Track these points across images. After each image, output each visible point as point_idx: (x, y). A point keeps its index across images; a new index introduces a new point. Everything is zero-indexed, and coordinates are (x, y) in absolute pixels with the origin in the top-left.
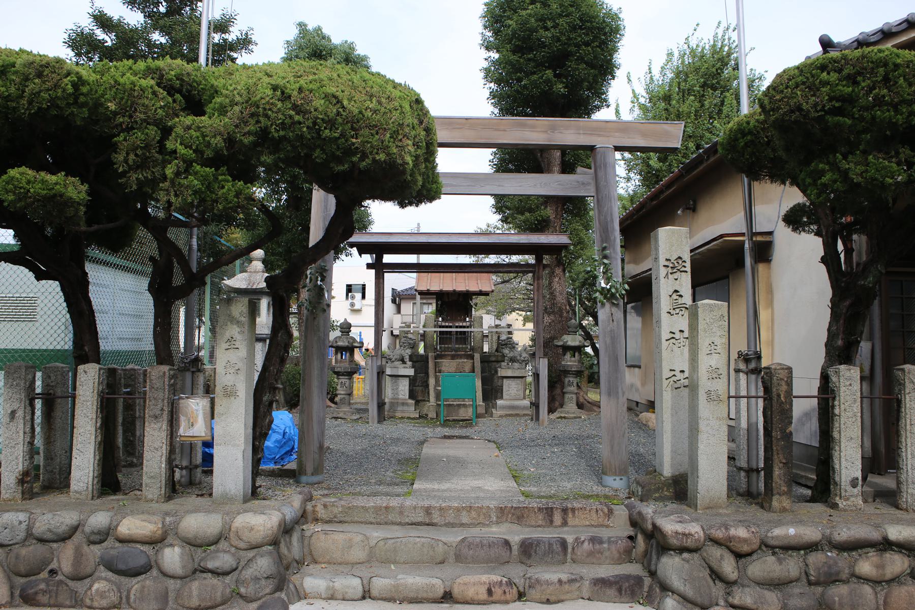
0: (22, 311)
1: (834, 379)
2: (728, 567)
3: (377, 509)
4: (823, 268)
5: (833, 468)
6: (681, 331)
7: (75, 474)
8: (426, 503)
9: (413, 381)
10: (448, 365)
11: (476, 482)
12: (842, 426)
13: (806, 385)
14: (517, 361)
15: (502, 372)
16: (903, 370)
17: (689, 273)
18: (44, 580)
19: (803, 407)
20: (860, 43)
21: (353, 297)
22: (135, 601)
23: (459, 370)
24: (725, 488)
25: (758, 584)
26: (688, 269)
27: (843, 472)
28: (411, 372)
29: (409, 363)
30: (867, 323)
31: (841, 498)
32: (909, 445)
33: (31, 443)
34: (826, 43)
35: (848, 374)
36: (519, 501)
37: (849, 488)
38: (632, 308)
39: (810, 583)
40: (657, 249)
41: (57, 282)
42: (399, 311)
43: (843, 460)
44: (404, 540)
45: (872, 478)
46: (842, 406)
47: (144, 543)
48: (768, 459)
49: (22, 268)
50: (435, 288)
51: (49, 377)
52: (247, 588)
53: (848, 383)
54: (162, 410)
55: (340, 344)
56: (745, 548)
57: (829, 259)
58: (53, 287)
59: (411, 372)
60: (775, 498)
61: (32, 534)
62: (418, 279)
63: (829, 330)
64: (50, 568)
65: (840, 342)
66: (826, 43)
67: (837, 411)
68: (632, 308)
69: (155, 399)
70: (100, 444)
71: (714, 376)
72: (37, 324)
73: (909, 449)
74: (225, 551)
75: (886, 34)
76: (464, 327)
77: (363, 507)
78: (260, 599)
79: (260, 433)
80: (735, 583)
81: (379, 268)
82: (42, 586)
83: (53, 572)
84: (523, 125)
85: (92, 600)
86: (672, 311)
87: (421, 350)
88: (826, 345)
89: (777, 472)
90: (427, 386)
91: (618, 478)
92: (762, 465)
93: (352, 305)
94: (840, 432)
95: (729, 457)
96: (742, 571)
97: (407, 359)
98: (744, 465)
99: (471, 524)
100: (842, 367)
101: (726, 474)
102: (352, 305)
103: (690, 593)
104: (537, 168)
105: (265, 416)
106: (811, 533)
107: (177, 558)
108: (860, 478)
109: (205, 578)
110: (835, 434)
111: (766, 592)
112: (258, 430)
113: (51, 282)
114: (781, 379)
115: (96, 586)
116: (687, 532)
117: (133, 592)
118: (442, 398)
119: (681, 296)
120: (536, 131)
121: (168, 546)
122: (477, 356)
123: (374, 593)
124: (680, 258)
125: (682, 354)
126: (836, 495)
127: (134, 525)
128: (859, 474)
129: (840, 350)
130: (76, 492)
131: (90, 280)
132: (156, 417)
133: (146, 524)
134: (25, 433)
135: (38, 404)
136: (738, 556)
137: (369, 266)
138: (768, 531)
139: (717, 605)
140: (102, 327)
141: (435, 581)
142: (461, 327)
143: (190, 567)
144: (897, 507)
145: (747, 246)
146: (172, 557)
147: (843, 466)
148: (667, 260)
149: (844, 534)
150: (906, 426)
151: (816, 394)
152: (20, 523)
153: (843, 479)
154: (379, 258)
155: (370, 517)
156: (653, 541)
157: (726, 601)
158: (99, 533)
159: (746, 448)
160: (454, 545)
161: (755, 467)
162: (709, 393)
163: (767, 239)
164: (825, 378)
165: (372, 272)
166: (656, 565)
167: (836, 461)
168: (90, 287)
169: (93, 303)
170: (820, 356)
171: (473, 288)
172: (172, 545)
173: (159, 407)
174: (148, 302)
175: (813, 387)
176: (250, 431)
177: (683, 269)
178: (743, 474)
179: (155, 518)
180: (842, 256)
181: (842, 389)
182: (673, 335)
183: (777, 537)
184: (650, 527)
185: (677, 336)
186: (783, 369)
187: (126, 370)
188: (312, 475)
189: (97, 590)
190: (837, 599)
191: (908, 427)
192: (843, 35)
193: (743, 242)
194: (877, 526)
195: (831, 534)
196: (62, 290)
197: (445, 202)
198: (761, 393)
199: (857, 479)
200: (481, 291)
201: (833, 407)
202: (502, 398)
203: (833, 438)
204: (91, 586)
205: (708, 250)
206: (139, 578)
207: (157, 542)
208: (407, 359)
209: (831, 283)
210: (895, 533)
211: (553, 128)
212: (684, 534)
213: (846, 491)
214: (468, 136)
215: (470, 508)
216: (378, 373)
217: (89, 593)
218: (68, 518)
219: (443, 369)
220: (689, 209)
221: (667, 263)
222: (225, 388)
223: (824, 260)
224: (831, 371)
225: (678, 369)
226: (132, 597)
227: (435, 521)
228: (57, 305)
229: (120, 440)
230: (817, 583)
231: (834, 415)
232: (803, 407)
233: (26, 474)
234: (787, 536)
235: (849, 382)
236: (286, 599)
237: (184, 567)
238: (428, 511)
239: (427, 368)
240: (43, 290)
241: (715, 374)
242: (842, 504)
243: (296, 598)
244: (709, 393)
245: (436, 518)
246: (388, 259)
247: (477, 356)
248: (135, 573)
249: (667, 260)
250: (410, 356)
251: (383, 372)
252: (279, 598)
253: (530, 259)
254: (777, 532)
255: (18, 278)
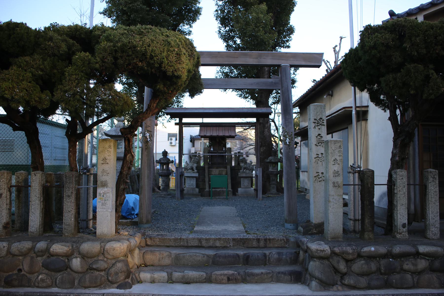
0: (7, 146)
1: (394, 176)
2: (342, 267)
3: (175, 240)
4: (389, 122)
5: (394, 219)
6: (322, 154)
7: (31, 223)
8: (199, 237)
9: (197, 179)
10: (215, 171)
11: (225, 227)
12: (398, 199)
13: (381, 178)
14: (248, 169)
15: (240, 175)
16: (428, 171)
17: (326, 126)
18: (16, 274)
19: (380, 191)
20: (410, 13)
21: (171, 139)
22: (59, 284)
23: (220, 174)
24: (342, 229)
25: (358, 275)
26: (325, 124)
27: (399, 220)
28: (197, 175)
29: (196, 171)
30: (411, 148)
31: (397, 233)
32: (430, 207)
33: (10, 209)
34: (392, 13)
35: (401, 173)
36: (244, 236)
37: (401, 228)
38: (304, 143)
39: (381, 274)
40: (310, 114)
41: (24, 132)
42: (193, 146)
43: (399, 215)
44: (188, 254)
45: (414, 224)
46: (398, 189)
47: (63, 256)
48: (362, 214)
49: (7, 125)
50: (208, 134)
51: (19, 178)
52: (112, 277)
53: (401, 178)
54: (72, 193)
55: (162, 161)
56: (351, 257)
57: (393, 119)
58: (22, 134)
59: (197, 175)
60: (366, 233)
61: (10, 252)
62: (200, 130)
63: (392, 152)
64: (18, 268)
65: (397, 158)
66: (392, 13)
67: (396, 191)
68: (304, 143)
69: (68, 187)
70: (42, 209)
71: (336, 175)
72: (14, 153)
73: (430, 209)
74: (102, 260)
75: (421, 9)
76: (223, 153)
77: (169, 239)
78: (118, 282)
79: (119, 204)
80: (345, 274)
81: (181, 125)
82: (15, 277)
83: (20, 270)
84: (245, 55)
85: (38, 283)
86: (317, 144)
87: (202, 164)
88: (391, 160)
89: (367, 221)
90: (205, 182)
91: (292, 225)
92: (360, 218)
93: (171, 143)
94: (397, 201)
95: (344, 213)
96: (349, 267)
97: (195, 168)
98: (352, 218)
99: (221, 247)
100: (398, 170)
101: (342, 222)
102: (171, 143)
103: (324, 278)
104: (258, 76)
105: (121, 196)
106: (382, 250)
107: (79, 263)
108: (407, 224)
109: (92, 273)
110: (395, 203)
111: (360, 278)
112: (118, 202)
113: (20, 132)
114: (369, 176)
115: (40, 277)
116: (322, 249)
117: (58, 279)
118: (211, 187)
119: (322, 137)
120: (252, 58)
121: (75, 258)
122: (229, 167)
123: (174, 279)
124: (321, 118)
125: (322, 165)
126: (395, 232)
127: (58, 248)
128: (406, 221)
129: (398, 161)
130: (31, 232)
131: (39, 131)
132: (69, 196)
133: (64, 247)
134: (7, 204)
135: (14, 189)
136: (347, 261)
137: (176, 124)
138: (361, 249)
139: (337, 284)
140: (46, 153)
141: (202, 273)
142: (221, 153)
143: (86, 267)
144: (426, 237)
145: (354, 112)
146: (76, 263)
147: (399, 218)
148: (315, 119)
149: (397, 249)
150: (429, 198)
151: (386, 183)
152: (4, 247)
153: (399, 224)
154: (181, 120)
155: (172, 243)
156: (307, 254)
157: (341, 283)
158: (42, 251)
159: (353, 209)
160: (212, 257)
161: (357, 218)
162: (334, 183)
163: (366, 109)
164: (390, 175)
165: (178, 126)
166: (308, 265)
167: (395, 215)
168: (39, 135)
169: (41, 142)
170: (388, 165)
171: (227, 134)
172: (76, 257)
173: (70, 192)
174: (66, 142)
175: (385, 180)
176: (114, 203)
177: (323, 124)
178: (352, 222)
179: (68, 244)
180: (399, 117)
181: (398, 181)
182: (318, 156)
183: (366, 252)
184: (305, 247)
185: (320, 156)
186: (369, 171)
187: (57, 174)
188: (146, 224)
189: (41, 279)
190: (394, 281)
191: (430, 199)
192: (399, 11)
193: (352, 111)
194: (415, 246)
195: (391, 250)
196: (26, 135)
197: (206, 92)
198: (357, 182)
199: (405, 224)
200: (230, 135)
201: (394, 189)
202: (240, 187)
203: (394, 204)
204: (38, 277)
205: (337, 115)
206: (61, 273)
207: (69, 256)
208: (195, 168)
209: (393, 129)
210: (422, 249)
211: (260, 56)
212: (321, 251)
213: (400, 230)
214: (213, 59)
215: (220, 239)
216: (180, 176)
217: (37, 280)
218: (27, 245)
219: (213, 173)
220: (329, 95)
221: (315, 121)
222: (102, 182)
223: (390, 119)
224: (393, 173)
225: (320, 172)
226: (58, 282)
227: (204, 245)
228: (23, 143)
229: (54, 208)
230: (385, 274)
231: (394, 193)
232: (380, 191)
233: (7, 224)
234: (370, 251)
235: (402, 177)
236: (131, 282)
237: (82, 267)
238: (200, 240)
239: (205, 172)
240: (16, 136)
241: (336, 174)
242: (398, 236)
243: (136, 282)
244: (334, 183)
245: (204, 243)
246: (185, 120)
247: (229, 167)
248: (59, 270)
249: (315, 119)
250: (196, 167)
251: (183, 175)
252: (128, 282)
253: (254, 120)
254: (366, 249)
255: (4, 131)
